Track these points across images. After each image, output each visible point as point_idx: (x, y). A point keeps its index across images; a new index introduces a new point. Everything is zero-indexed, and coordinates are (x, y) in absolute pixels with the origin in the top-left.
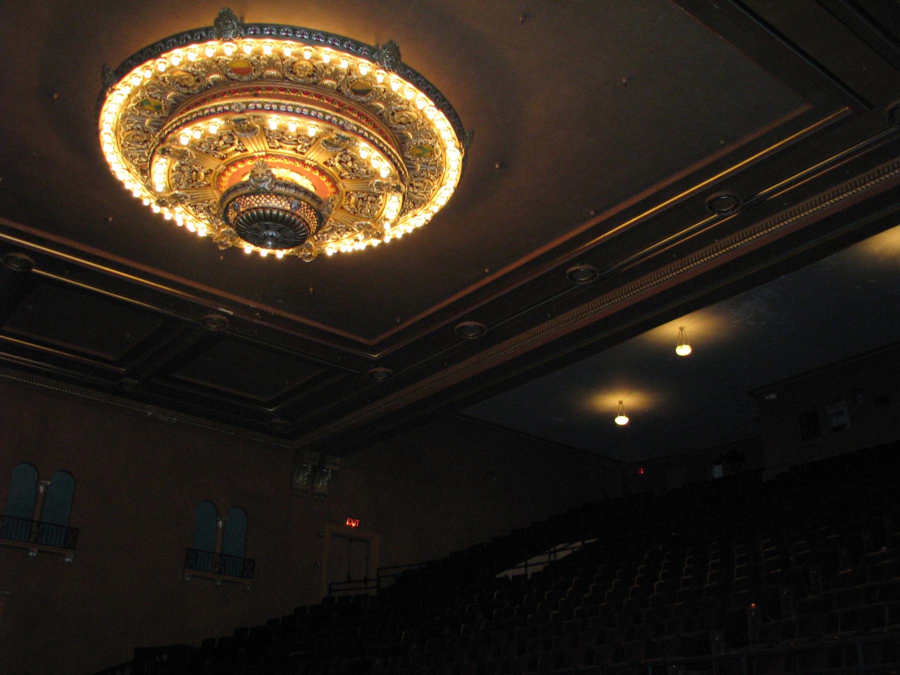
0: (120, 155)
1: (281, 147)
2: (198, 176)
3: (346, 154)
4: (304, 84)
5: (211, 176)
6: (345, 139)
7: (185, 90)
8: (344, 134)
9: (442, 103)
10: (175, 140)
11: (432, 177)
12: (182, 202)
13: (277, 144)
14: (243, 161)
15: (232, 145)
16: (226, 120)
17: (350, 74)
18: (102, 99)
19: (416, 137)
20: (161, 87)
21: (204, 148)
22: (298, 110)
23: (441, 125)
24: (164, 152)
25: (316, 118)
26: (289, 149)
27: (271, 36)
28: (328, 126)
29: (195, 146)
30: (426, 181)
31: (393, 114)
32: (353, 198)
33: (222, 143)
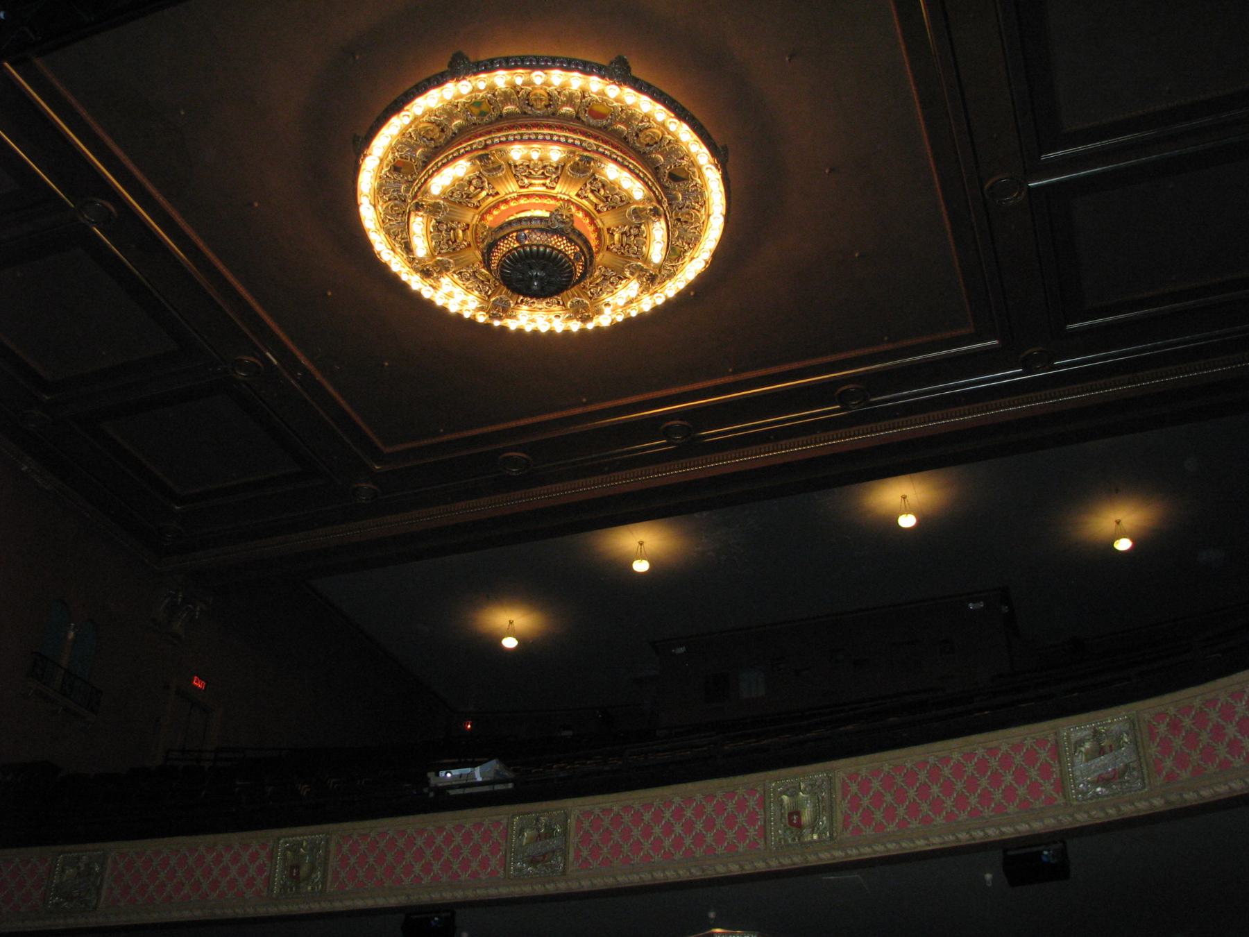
0: (382, 233)
1: (531, 185)
2: (456, 236)
3: (595, 179)
4: (543, 116)
5: (469, 232)
6: (589, 160)
7: (432, 144)
8: (586, 154)
9: (681, 113)
10: (426, 192)
11: (697, 206)
12: (447, 270)
13: (526, 181)
14: (496, 206)
15: (482, 189)
16: (470, 160)
17: (584, 97)
18: (356, 169)
19: (685, 199)
20: (408, 145)
21: (457, 196)
22: (540, 137)
23: (684, 134)
24: (418, 207)
25: (559, 142)
26: (534, 183)
27: (501, 68)
28: (571, 148)
29: (449, 195)
30: (692, 212)
31: (637, 135)
32: (617, 236)
33: (472, 188)
